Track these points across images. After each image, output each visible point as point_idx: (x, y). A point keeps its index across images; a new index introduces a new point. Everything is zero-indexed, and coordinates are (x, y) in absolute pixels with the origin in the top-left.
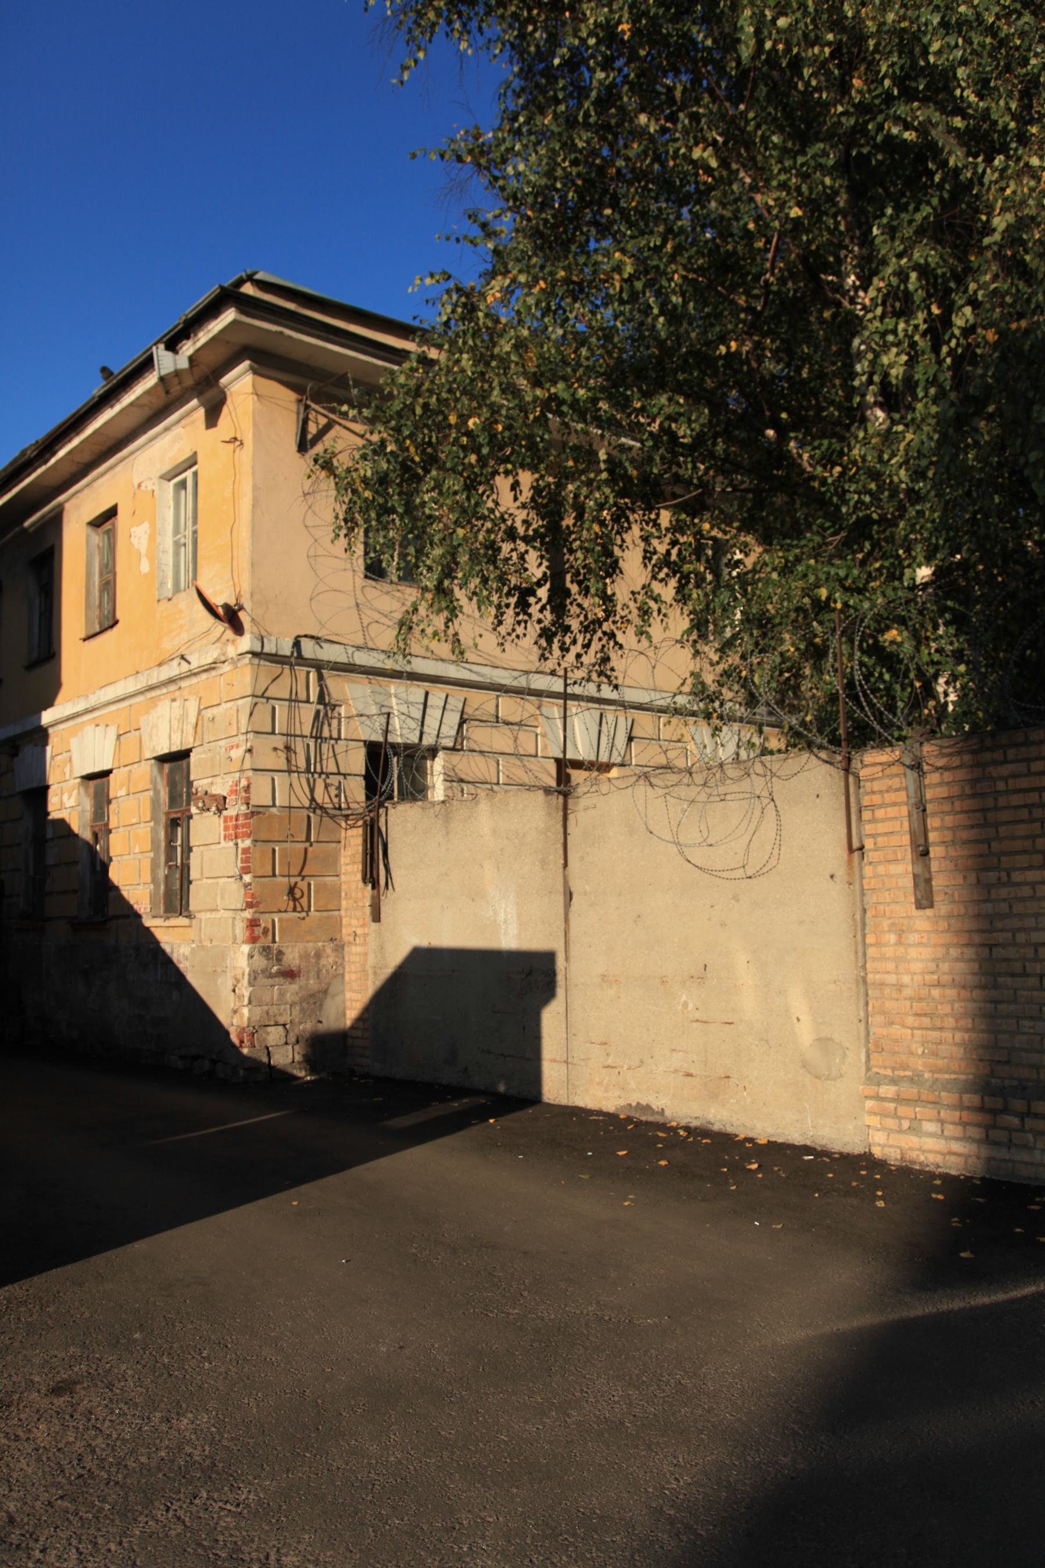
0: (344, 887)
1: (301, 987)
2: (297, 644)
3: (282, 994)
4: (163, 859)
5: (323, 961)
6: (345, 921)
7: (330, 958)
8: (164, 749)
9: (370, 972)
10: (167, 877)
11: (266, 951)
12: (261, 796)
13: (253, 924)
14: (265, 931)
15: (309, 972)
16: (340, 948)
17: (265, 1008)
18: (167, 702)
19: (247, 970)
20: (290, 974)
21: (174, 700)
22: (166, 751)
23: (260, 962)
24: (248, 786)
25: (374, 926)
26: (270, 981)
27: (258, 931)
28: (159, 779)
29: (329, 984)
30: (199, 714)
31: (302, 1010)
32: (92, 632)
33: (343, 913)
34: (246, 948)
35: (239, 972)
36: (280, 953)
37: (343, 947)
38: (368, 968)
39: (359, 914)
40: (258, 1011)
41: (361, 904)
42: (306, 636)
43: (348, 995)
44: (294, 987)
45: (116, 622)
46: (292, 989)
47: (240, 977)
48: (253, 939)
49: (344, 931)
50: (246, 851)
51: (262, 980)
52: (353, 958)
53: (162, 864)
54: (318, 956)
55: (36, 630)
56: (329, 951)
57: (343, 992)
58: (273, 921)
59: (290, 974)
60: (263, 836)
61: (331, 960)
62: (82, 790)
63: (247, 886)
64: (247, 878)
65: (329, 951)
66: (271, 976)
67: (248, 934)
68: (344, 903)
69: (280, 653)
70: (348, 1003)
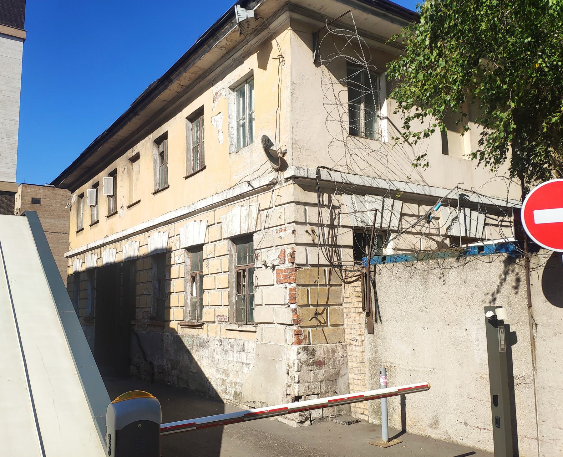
0: (345, 310)
1: (325, 371)
2: (318, 172)
3: (316, 376)
4: (235, 292)
5: (336, 355)
6: (346, 331)
7: (340, 353)
8: (236, 232)
9: (367, 363)
10: (237, 301)
11: (306, 349)
12: (300, 259)
13: (298, 333)
14: (305, 337)
15: (329, 362)
16: (344, 347)
17: (307, 384)
18: (239, 208)
19: (296, 362)
20: (319, 364)
21: (242, 206)
22: (238, 233)
23: (303, 356)
24: (293, 252)
25: (369, 336)
26: (309, 368)
27: (301, 337)
28: (232, 248)
29: (340, 369)
30: (259, 213)
31: (327, 386)
32: (190, 174)
33: (345, 326)
34: (296, 348)
35: (291, 363)
36: (314, 350)
37: (346, 346)
38: (366, 360)
39: (357, 327)
40: (303, 386)
41: (358, 321)
42: (322, 167)
43: (351, 376)
44: (322, 371)
45: (205, 167)
46: (321, 373)
47: (292, 365)
48: (299, 342)
49: (346, 336)
50: (291, 290)
51: (305, 367)
52: (354, 354)
53: (234, 294)
54: (334, 352)
55: (158, 174)
56: (339, 348)
57: (347, 373)
58: (309, 332)
59: (319, 364)
60: (302, 282)
61: (340, 354)
62: (186, 254)
63: (294, 311)
64: (293, 306)
65: (339, 348)
66: (310, 365)
67: (295, 339)
68: (346, 321)
69: (310, 177)
70: (351, 381)
